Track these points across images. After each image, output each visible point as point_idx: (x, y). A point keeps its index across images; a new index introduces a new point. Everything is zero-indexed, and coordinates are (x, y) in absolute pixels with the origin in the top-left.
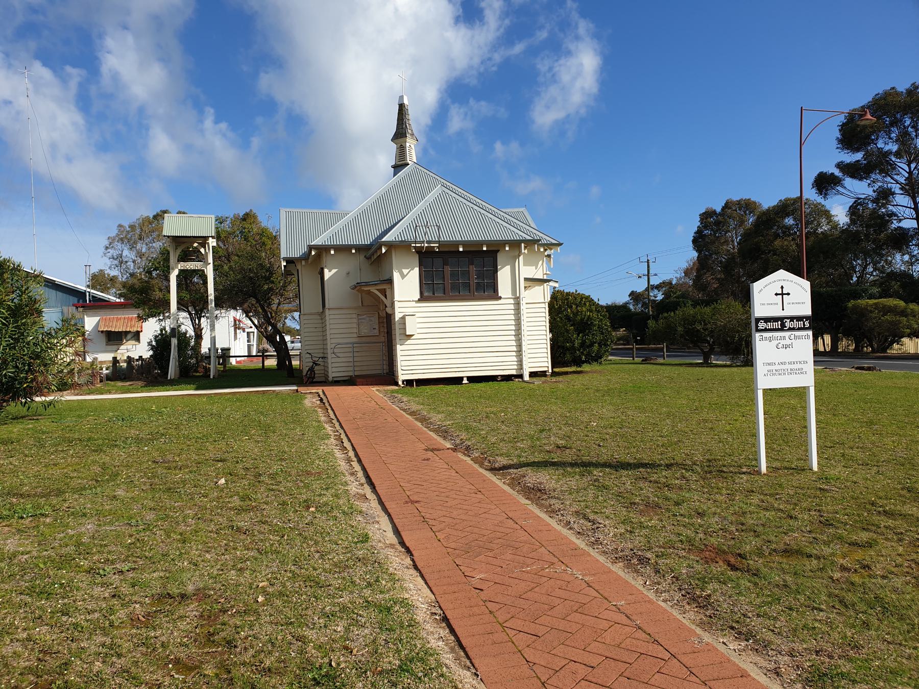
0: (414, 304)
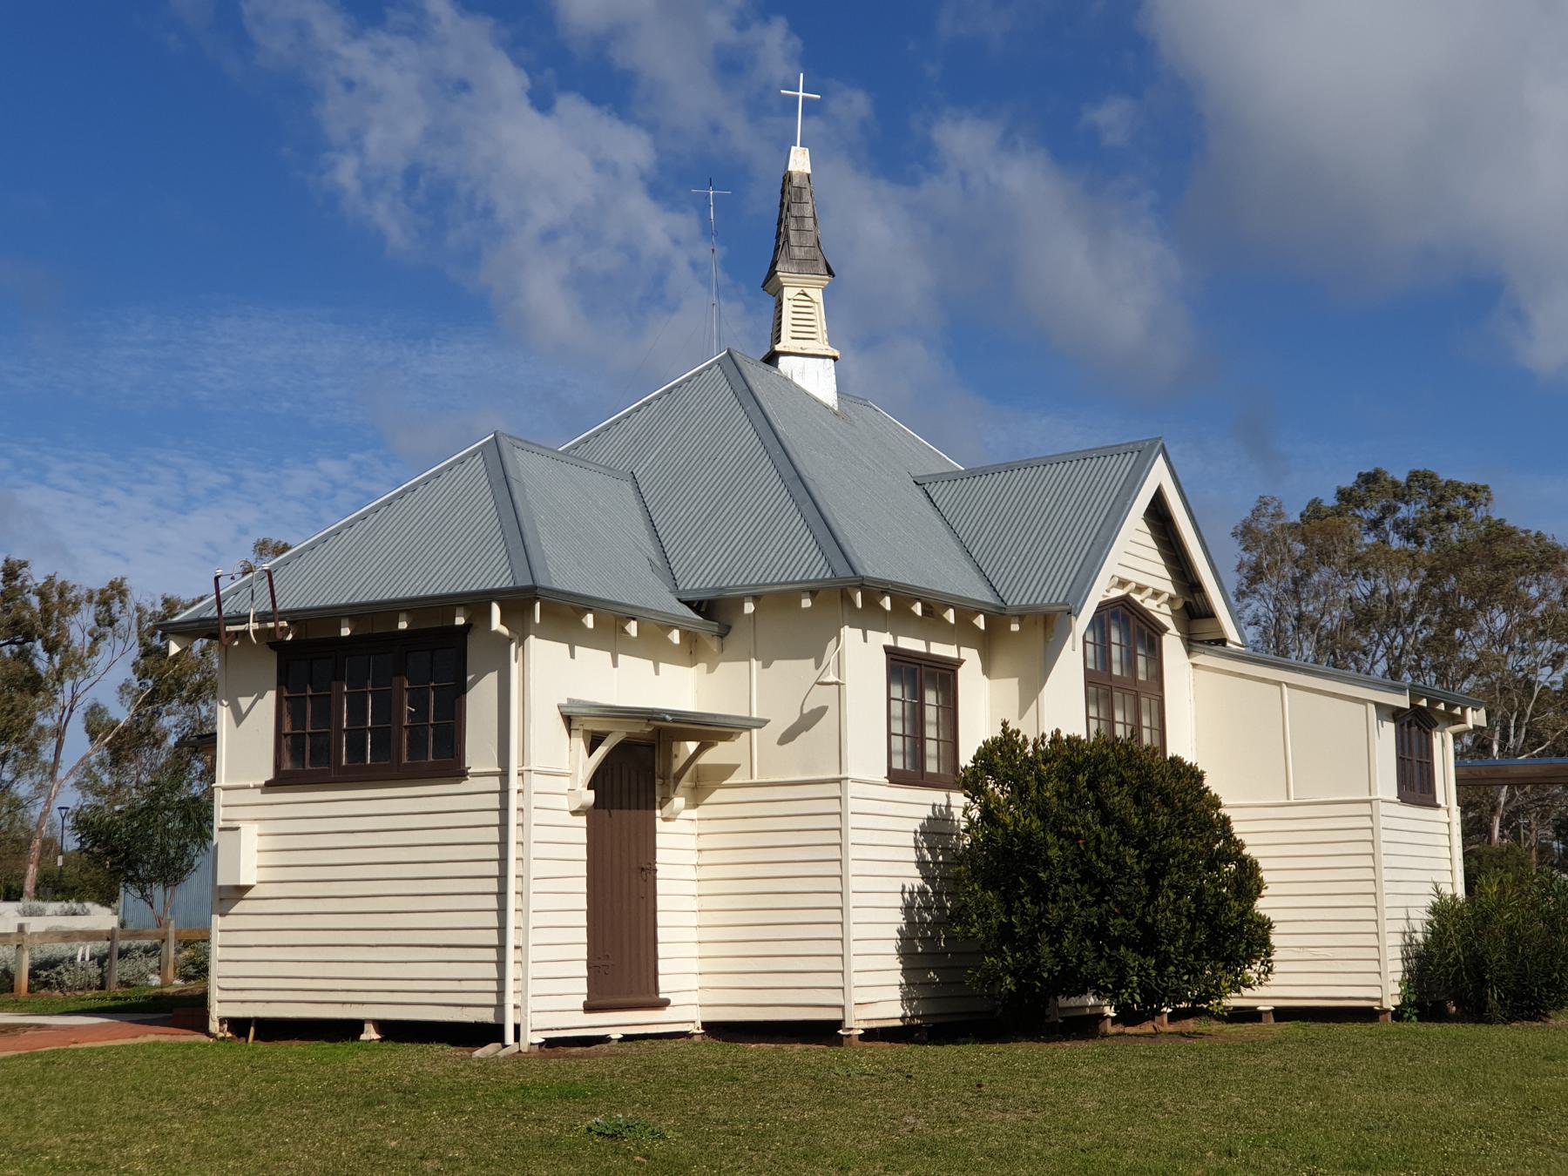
0: (257, 796)
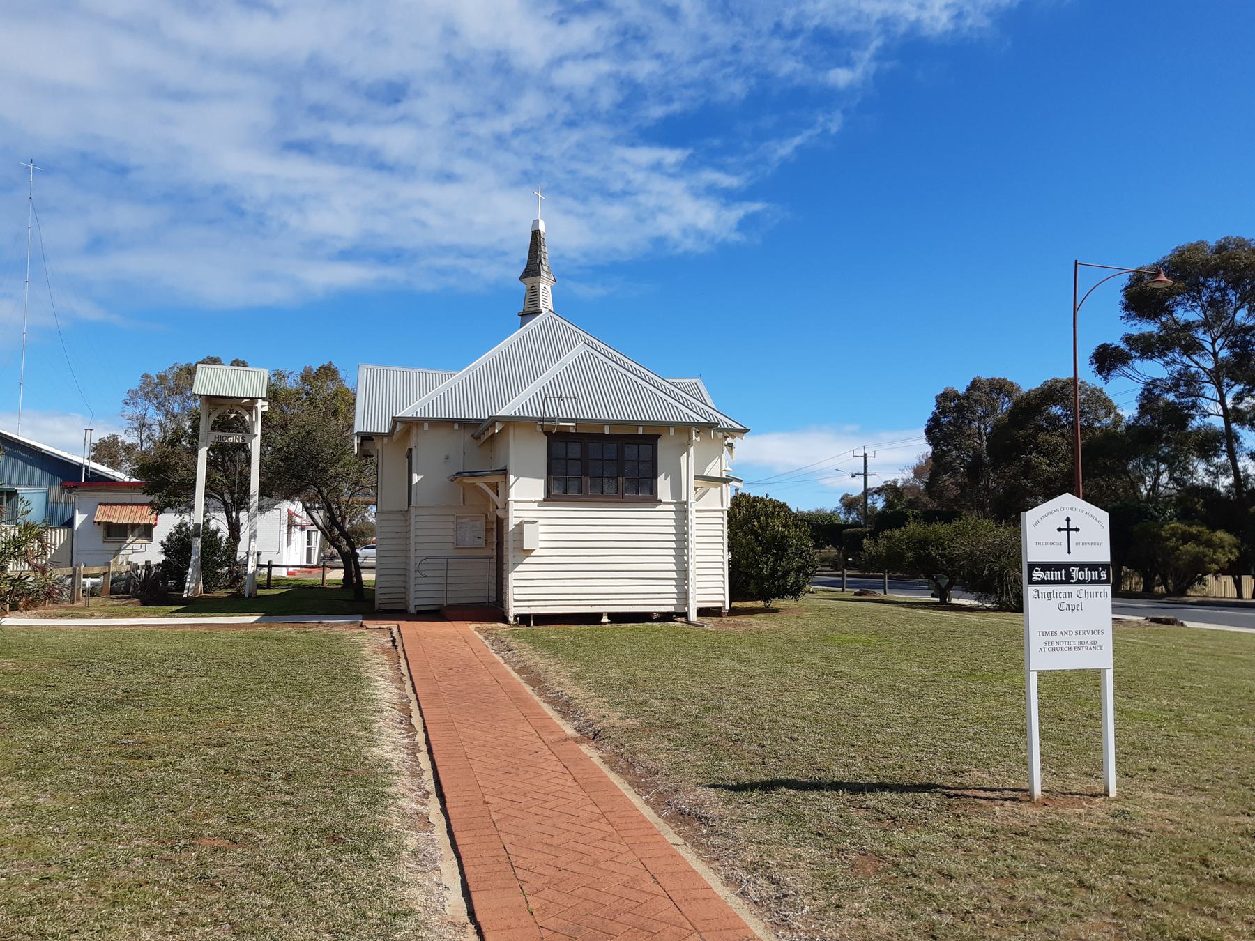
0: (535, 506)
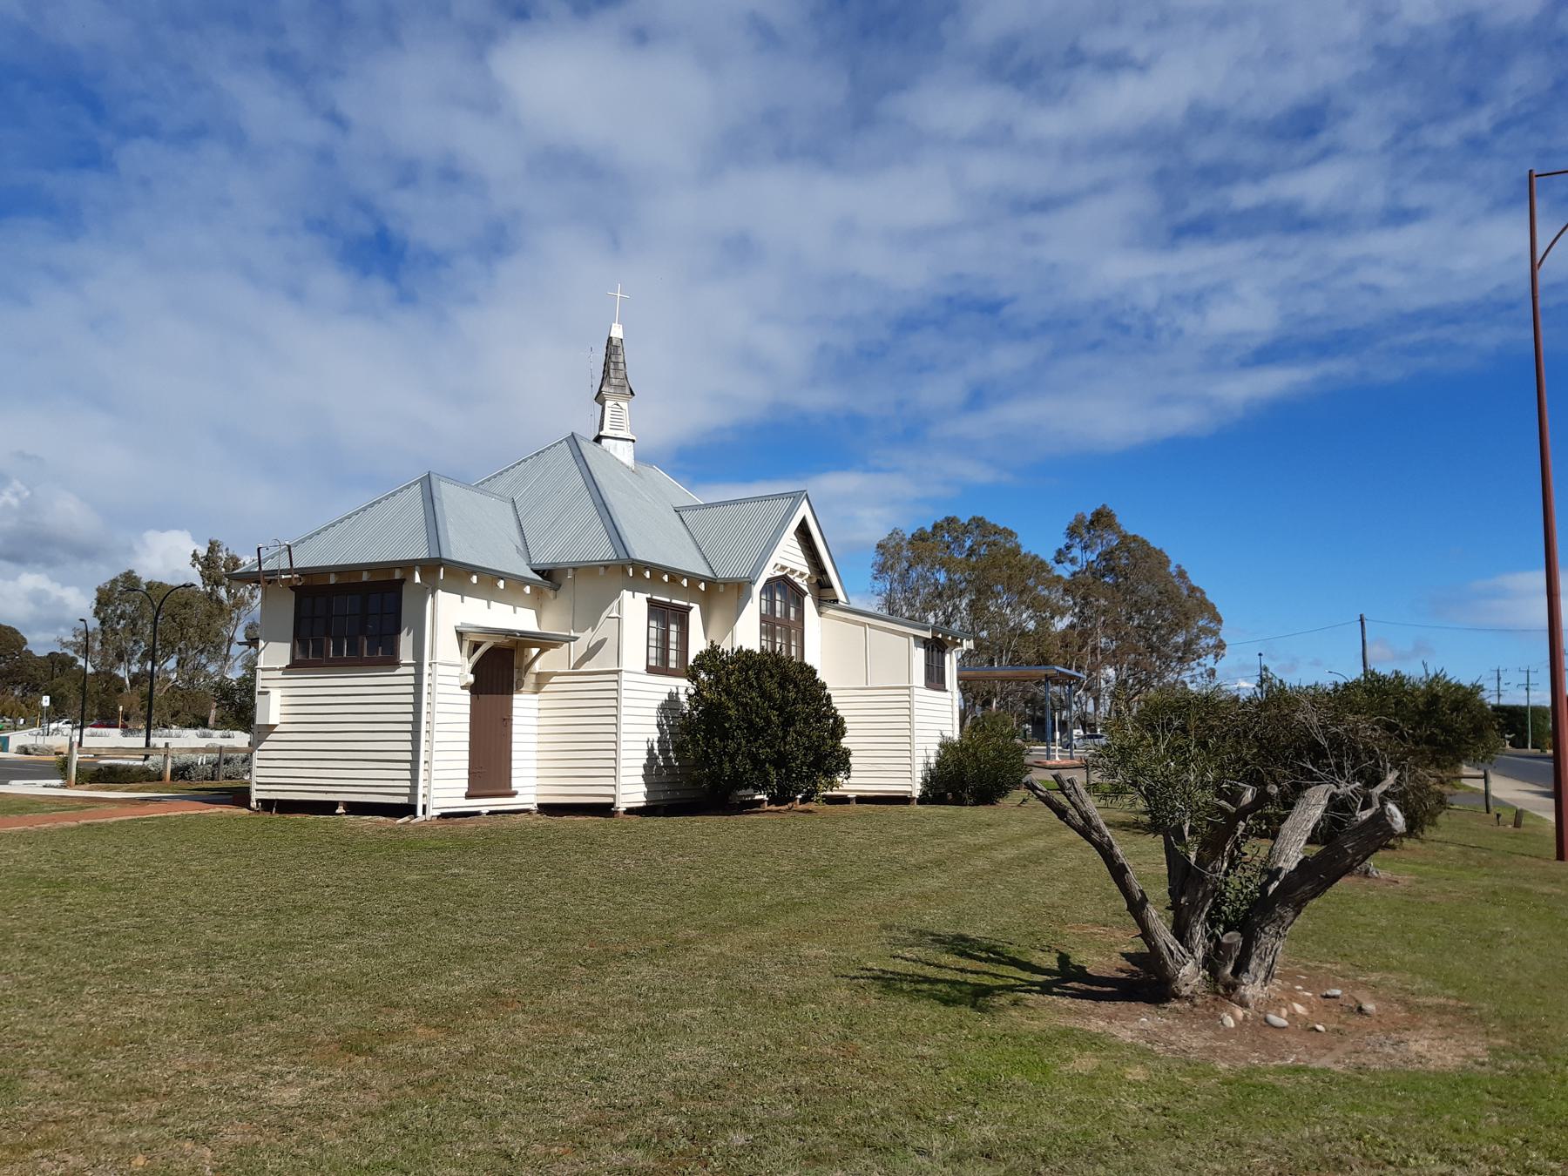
0: (279, 674)
